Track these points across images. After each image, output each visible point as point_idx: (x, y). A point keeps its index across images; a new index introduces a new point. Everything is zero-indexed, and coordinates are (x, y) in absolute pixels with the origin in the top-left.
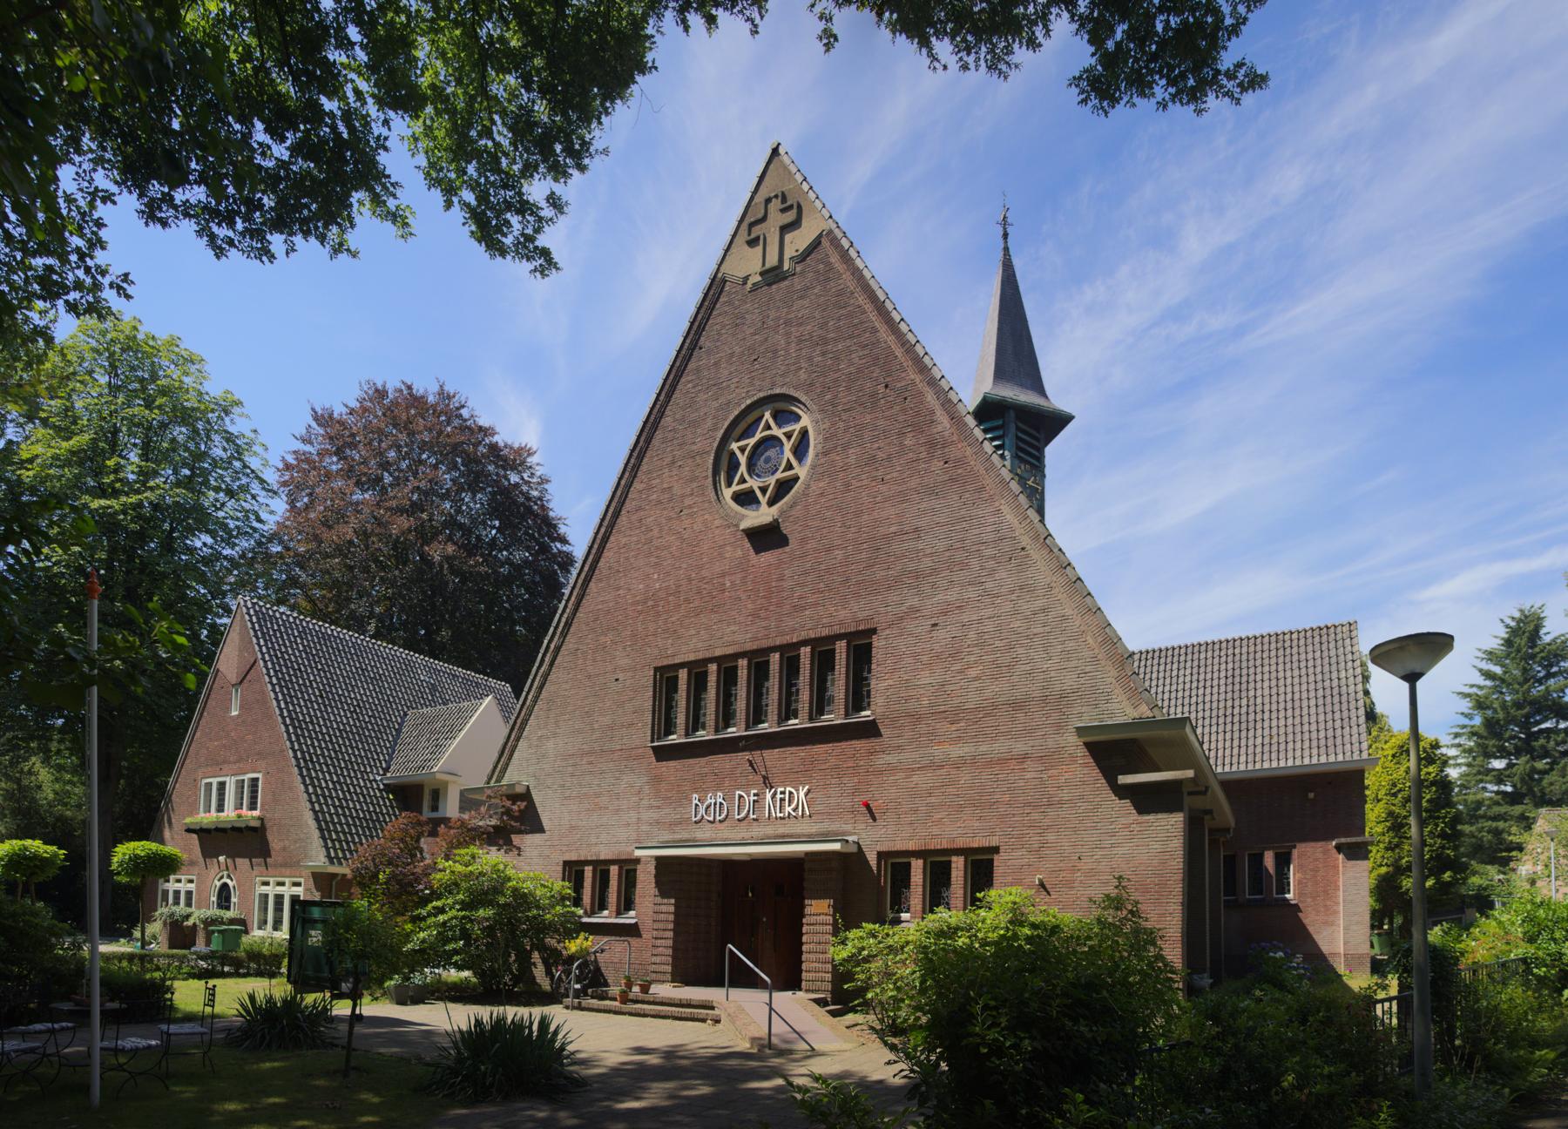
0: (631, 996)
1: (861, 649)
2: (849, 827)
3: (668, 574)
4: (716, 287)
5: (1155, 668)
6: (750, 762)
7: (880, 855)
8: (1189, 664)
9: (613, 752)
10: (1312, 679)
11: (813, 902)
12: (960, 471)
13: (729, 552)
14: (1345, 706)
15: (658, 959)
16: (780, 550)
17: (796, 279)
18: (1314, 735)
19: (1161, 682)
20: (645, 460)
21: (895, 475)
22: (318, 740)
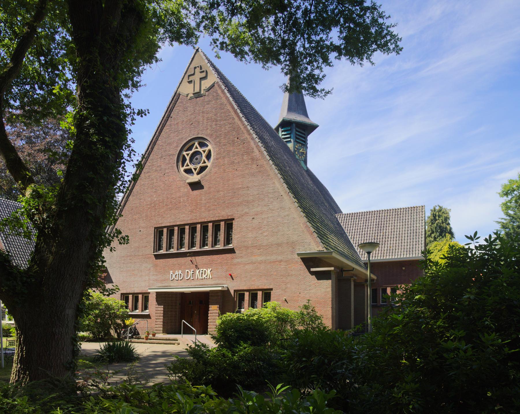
0: (149, 338)
1: (229, 225)
2: (225, 282)
3: (159, 195)
4: (177, 97)
5: (350, 220)
6: (191, 260)
7: (235, 291)
8: (363, 219)
9: (139, 256)
10: (407, 226)
11: (212, 306)
12: (262, 169)
13: (182, 190)
14: (417, 237)
15: (157, 326)
16: (201, 190)
17: (206, 97)
18: (406, 247)
19: (352, 226)
20: (151, 155)
21: (241, 168)
22: (17, 248)
